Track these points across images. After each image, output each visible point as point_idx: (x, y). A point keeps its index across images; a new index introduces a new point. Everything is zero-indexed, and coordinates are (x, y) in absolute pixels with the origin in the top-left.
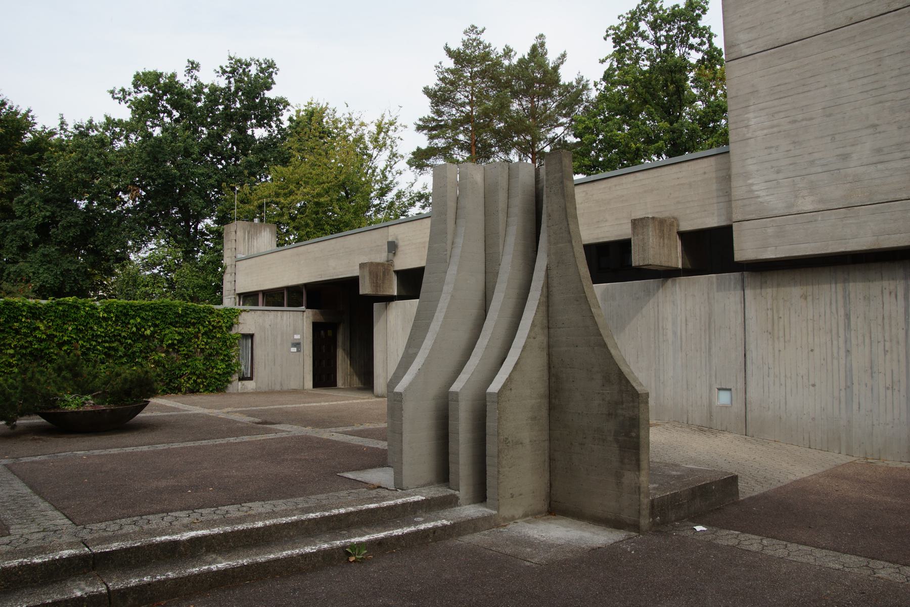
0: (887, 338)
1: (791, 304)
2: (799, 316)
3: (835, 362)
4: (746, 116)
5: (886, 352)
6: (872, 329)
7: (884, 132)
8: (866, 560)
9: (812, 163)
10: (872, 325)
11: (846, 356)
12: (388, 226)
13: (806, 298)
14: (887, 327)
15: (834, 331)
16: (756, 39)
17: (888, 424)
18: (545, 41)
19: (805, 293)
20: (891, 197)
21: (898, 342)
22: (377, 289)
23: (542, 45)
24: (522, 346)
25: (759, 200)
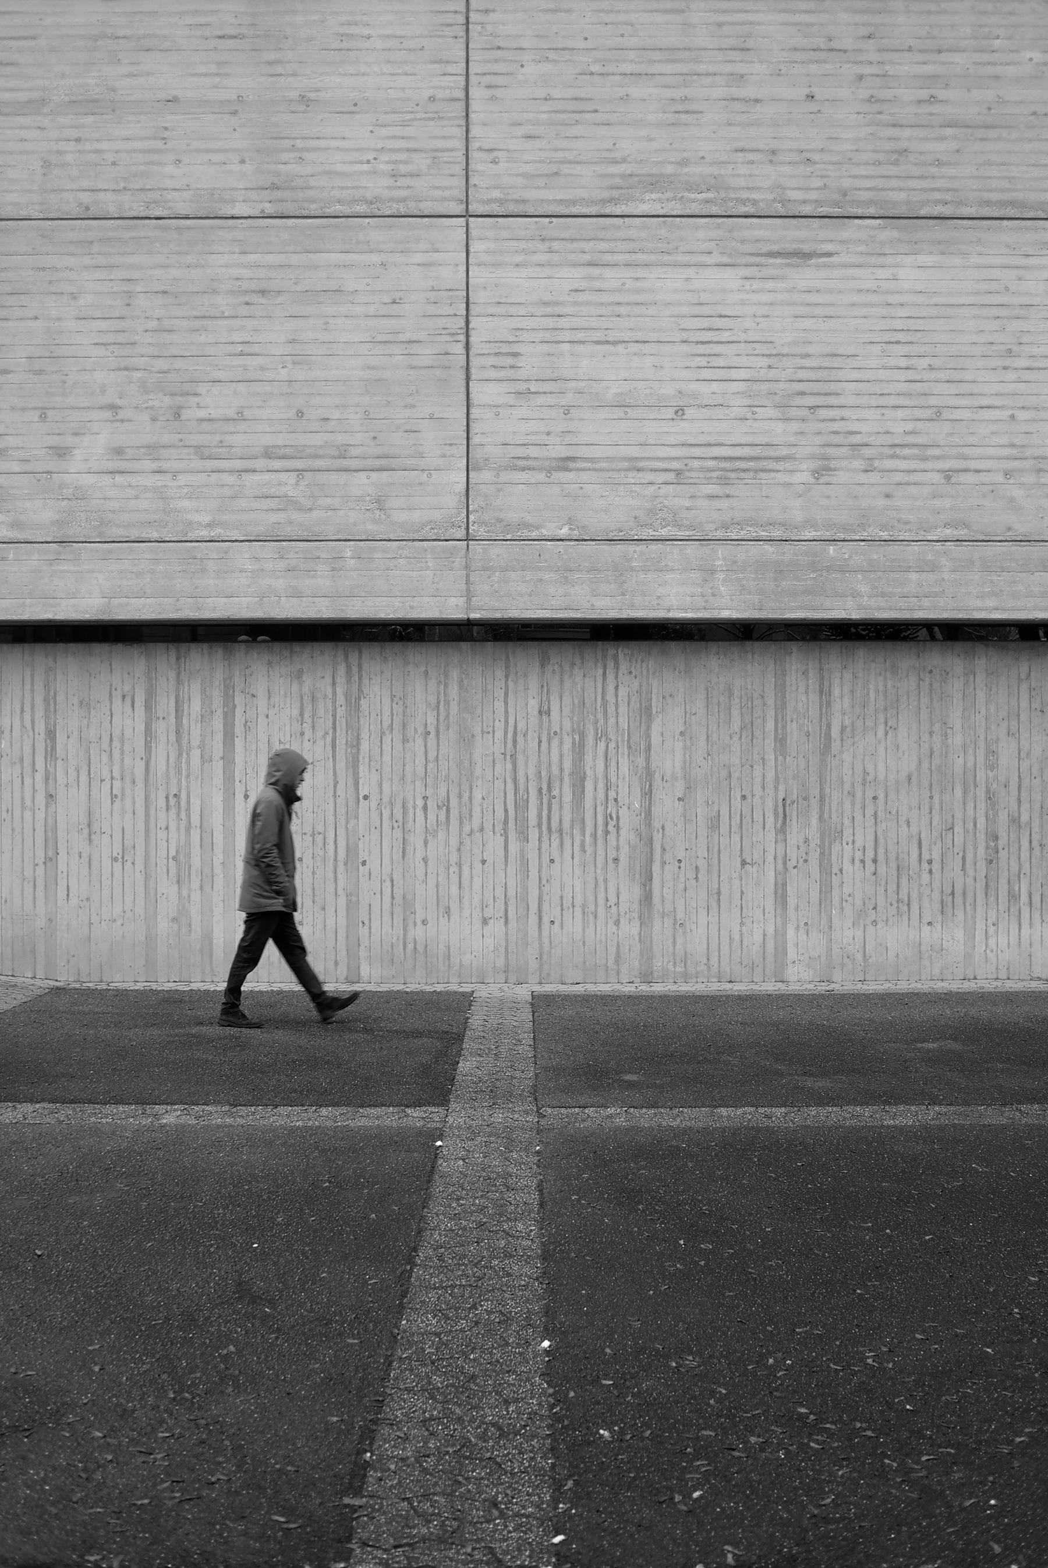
0: (116, 774)
3: (28, 815)
5: (113, 797)
6: (92, 756)
8: (140, 1107)
10: (92, 751)
11: (47, 806)
14: (116, 755)
15: (27, 762)
20: (135, 534)
21: (134, 782)
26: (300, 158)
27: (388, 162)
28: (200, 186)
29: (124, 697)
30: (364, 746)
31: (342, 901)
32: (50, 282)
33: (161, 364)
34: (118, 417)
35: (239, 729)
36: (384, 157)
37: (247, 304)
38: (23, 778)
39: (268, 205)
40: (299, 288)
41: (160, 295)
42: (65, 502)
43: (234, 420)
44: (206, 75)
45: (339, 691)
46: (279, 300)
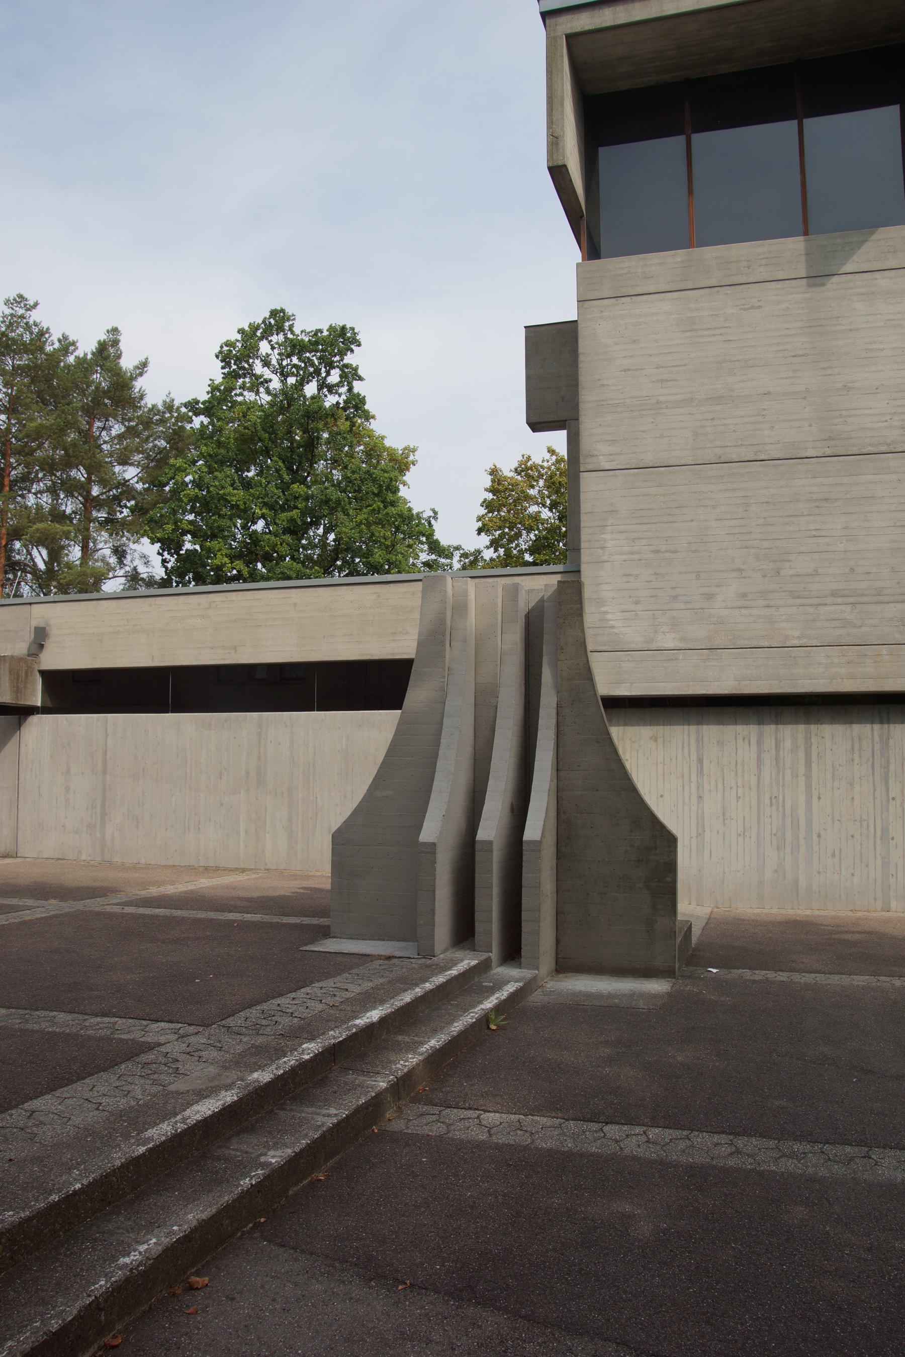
0: (740, 784)
1: (640, 746)
2: (648, 759)
4: (602, 536)
5: (738, 798)
7: (749, 577)
9: (675, 598)
11: (698, 803)
12: (30, 604)
13: (656, 740)
15: (686, 777)
16: (617, 454)
17: (739, 871)
18: (121, 338)
19: (655, 735)
20: (754, 644)
21: (750, 789)
22: (17, 696)
23: (116, 343)
24: (547, 790)
25: (614, 630)
26: (845, 421)
27: (899, 420)
28: (785, 441)
29: (744, 739)
30: (892, 768)
31: (879, 862)
32: (700, 500)
33: (766, 544)
34: (743, 575)
35: (814, 757)
36: (896, 418)
37: (817, 507)
38: (683, 787)
39: (827, 449)
40: (848, 496)
41: (765, 505)
42: (712, 625)
43: (812, 575)
44: (786, 378)
45: (876, 734)
46: (836, 504)
